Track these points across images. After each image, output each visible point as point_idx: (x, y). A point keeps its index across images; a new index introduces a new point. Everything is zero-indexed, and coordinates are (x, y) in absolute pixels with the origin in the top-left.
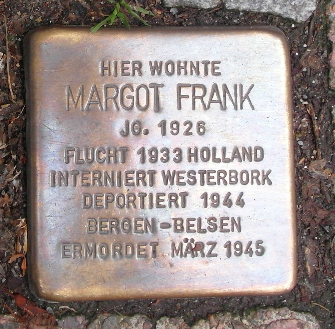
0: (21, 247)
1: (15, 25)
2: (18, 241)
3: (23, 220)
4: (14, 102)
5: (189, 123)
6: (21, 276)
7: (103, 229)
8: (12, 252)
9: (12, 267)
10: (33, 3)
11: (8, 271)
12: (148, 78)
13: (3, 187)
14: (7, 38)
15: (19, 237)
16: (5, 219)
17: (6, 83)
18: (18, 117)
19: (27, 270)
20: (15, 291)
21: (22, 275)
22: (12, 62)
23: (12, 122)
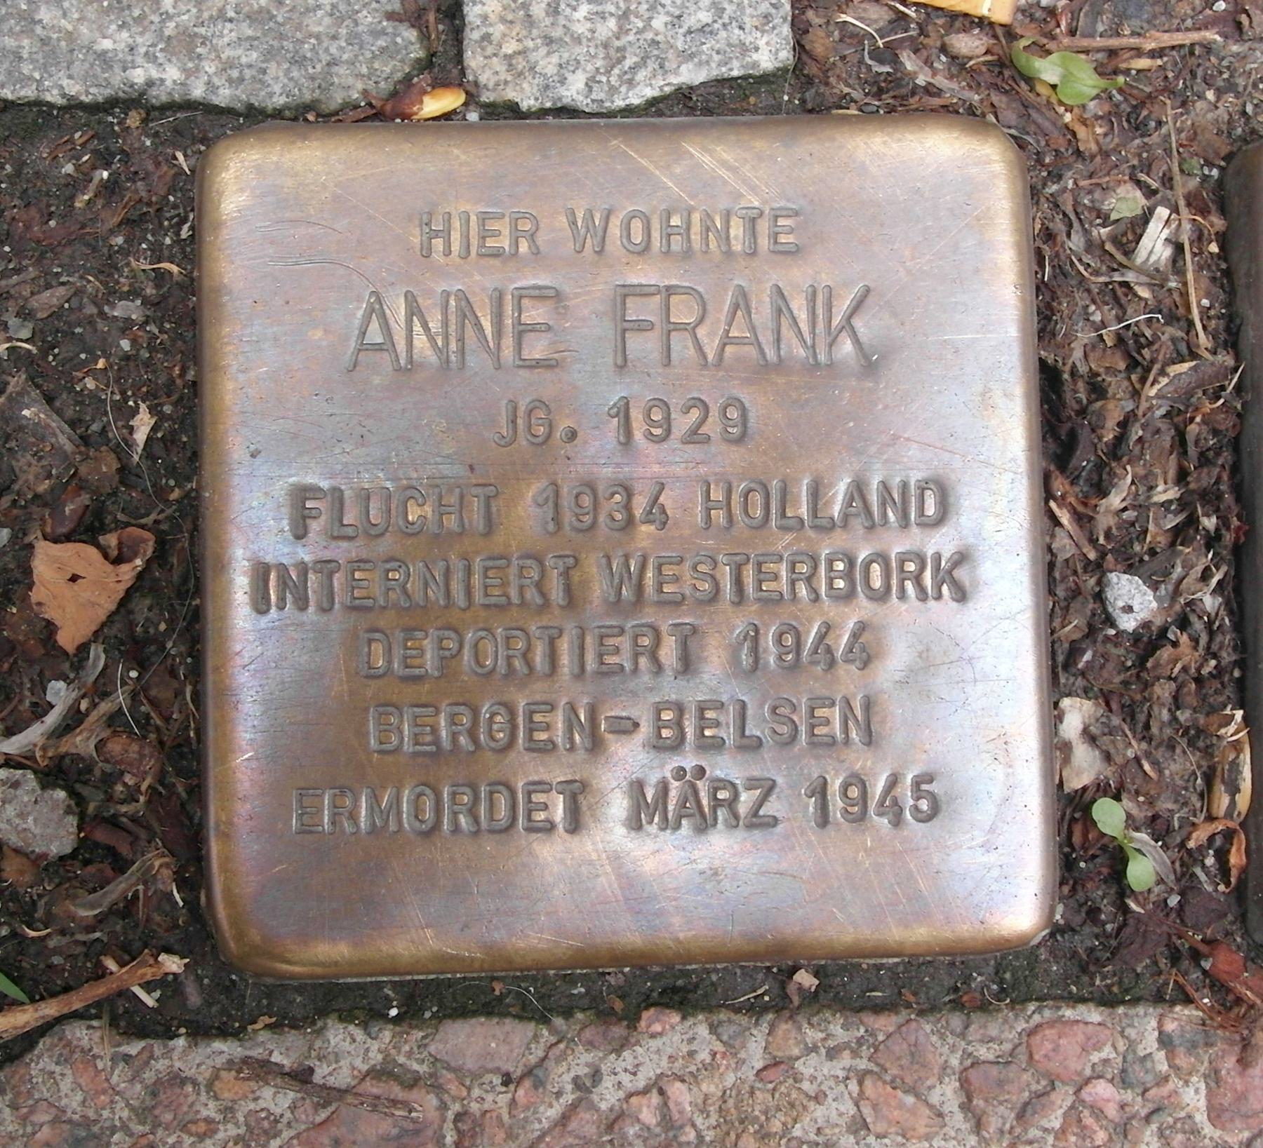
0: (1225, 800)
1: (1199, 131)
2: (1218, 781)
3: (1239, 714)
4: (1207, 355)
6: (1222, 888)
7: (707, 733)
8: (1195, 816)
9: (1195, 860)
10: (1252, 66)
11: (1183, 874)
13: (1169, 616)
14: (1176, 169)
15: (1219, 769)
16: (1178, 713)
17: (1178, 299)
18: (1222, 401)
19: (1244, 871)
20: (1209, 932)
21: (1228, 884)
22: (1199, 238)
23: (1198, 419)
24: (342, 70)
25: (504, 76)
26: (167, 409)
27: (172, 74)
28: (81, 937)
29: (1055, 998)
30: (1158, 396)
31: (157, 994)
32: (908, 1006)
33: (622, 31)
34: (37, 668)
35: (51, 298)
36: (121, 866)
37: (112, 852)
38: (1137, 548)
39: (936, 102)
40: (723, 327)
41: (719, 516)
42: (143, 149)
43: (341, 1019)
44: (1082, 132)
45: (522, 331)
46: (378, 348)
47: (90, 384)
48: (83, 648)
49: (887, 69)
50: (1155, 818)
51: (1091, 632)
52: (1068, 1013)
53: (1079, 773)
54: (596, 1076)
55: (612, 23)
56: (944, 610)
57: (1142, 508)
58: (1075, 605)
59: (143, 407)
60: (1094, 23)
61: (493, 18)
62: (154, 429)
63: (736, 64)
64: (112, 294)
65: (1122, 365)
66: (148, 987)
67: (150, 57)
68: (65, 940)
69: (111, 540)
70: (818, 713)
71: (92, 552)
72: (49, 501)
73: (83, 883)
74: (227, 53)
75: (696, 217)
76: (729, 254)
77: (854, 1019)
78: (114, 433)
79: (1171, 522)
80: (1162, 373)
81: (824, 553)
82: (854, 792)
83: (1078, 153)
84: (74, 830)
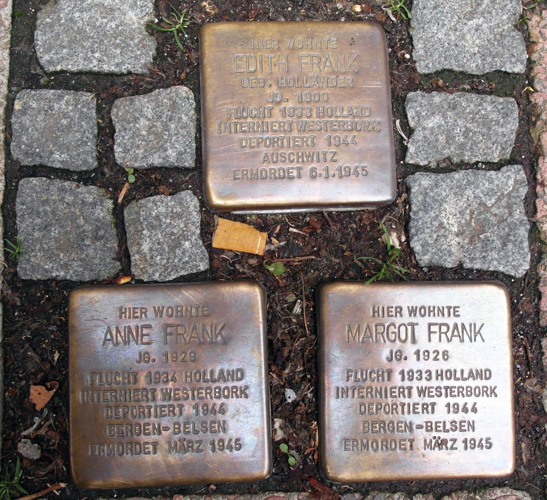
0: (313, 443)
3: (315, 423)
12: (406, 319)
19: (318, 459)
24: (102, 272)
25: (140, 273)
26: (62, 352)
27: (62, 274)
28: (42, 479)
29: (273, 491)
30: (297, 346)
31: (60, 492)
32: (238, 493)
33: (168, 263)
34: (31, 414)
35: (35, 326)
36: (51, 462)
37: (49, 458)
38: (293, 382)
39: (244, 276)
40: (190, 334)
41: (189, 379)
42: (56, 290)
43: (103, 498)
44: (280, 281)
45: (143, 335)
46: (109, 340)
47: (44, 346)
48: (42, 410)
49: (232, 268)
50: (298, 447)
51: (282, 402)
52: (276, 494)
53: (278, 437)
55: (165, 261)
56: (242, 400)
57: (294, 372)
58: (277, 396)
59: (57, 351)
60: (284, 254)
61: (137, 260)
62: (59, 356)
63: (194, 270)
64: (49, 324)
65: (289, 338)
66: (58, 490)
67: (57, 270)
68: (38, 479)
69: (48, 384)
70: (212, 425)
71: (44, 388)
72: (35, 374)
73: (42, 465)
74: (75, 268)
75: (184, 308)
76: (192, 316)
77: (224, 496)
78: (50, 358)
79: (301, 375)
80: (298, 340)
81: (213, 387)
82: (221, 444)
83: (279, 287)
84: (40, 453)
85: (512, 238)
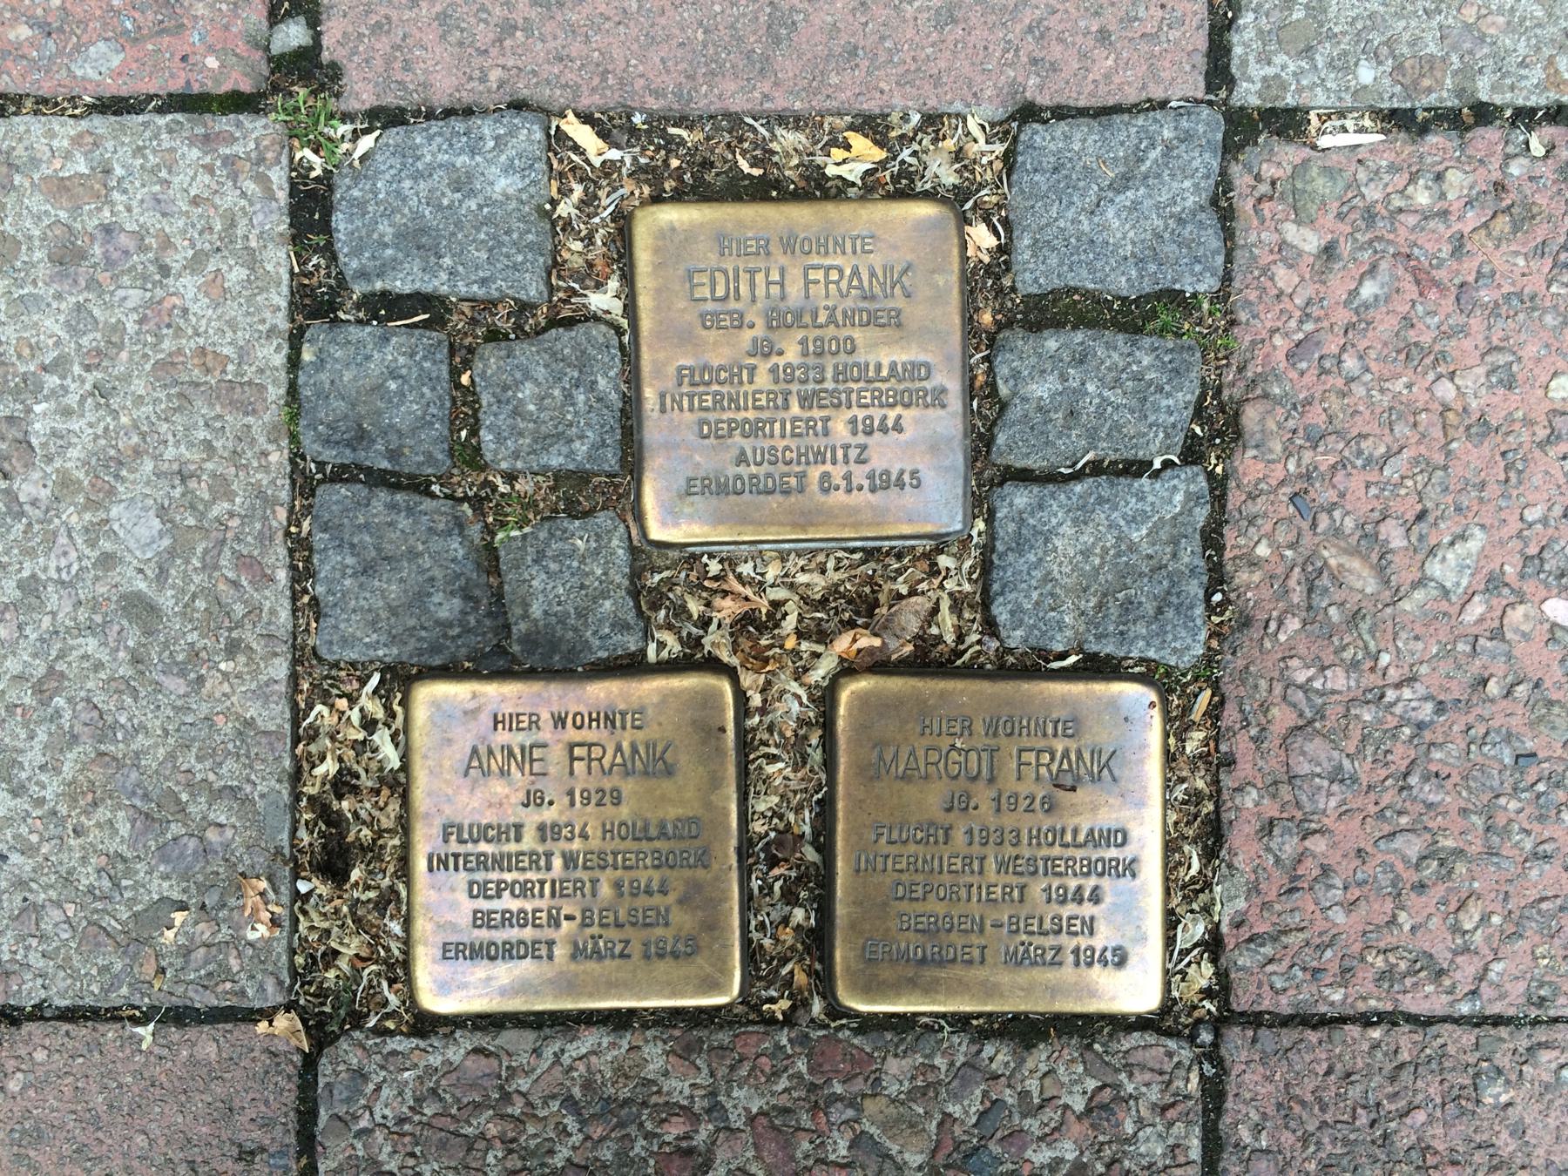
5: (601, 790)
12: (980, 741)
45: (532, 761)
54: (563, 1051)
56: (1125, 883)
85: (1174, 600)
